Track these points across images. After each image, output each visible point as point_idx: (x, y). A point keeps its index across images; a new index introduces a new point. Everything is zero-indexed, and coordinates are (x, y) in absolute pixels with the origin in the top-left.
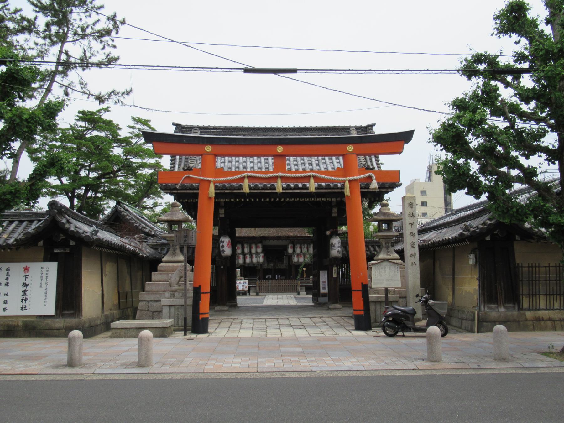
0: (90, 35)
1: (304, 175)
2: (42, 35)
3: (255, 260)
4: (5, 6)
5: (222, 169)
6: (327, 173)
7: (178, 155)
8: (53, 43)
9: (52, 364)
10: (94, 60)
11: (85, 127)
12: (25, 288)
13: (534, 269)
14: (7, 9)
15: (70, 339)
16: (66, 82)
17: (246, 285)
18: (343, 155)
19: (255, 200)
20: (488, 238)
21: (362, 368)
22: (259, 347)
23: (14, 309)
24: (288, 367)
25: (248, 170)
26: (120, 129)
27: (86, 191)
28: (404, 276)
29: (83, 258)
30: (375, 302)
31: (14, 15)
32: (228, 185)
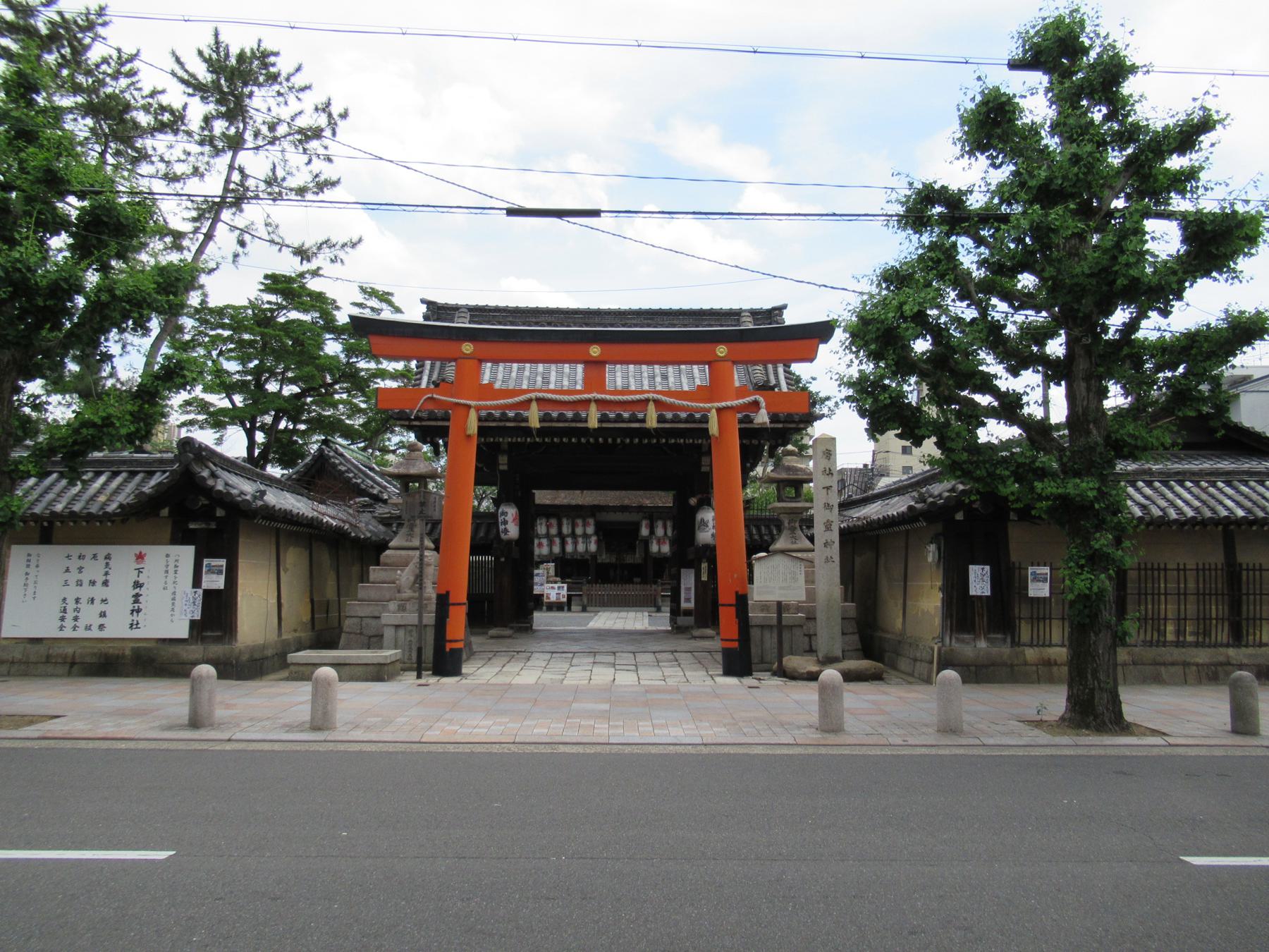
0: (284, 137)
1: (638, 397)
2: (197, 137)
3: (581, 548)
4: (133, 83)
5: (491, 384)
6: (680, 394)
7: (428, 359)
8: (217, 152)
9: (164, 722)
10: (292, 182)
11: (276, 304)
12: (137, 590)
13: (1213, 573)
14: (136, 89)
15: (194, 680)
16: (240, 221)
17: (564, 592)
18: (709, 363)
20: (959, 516)
21: (698, 741)
22: (537, 697)
23: (117, 627)
24: (572, 735)
25: (552, 386)
26: (338, 308)
27: (277, 420)
28: (810, 579)
29: (241, 540)
30: (762, 627)
31: (150, 100)
32: (511, 414)
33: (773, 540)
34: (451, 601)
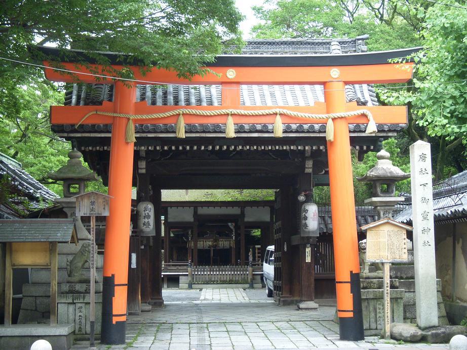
6: (307, 109)
18: (324, 84)
34: (116, 283)
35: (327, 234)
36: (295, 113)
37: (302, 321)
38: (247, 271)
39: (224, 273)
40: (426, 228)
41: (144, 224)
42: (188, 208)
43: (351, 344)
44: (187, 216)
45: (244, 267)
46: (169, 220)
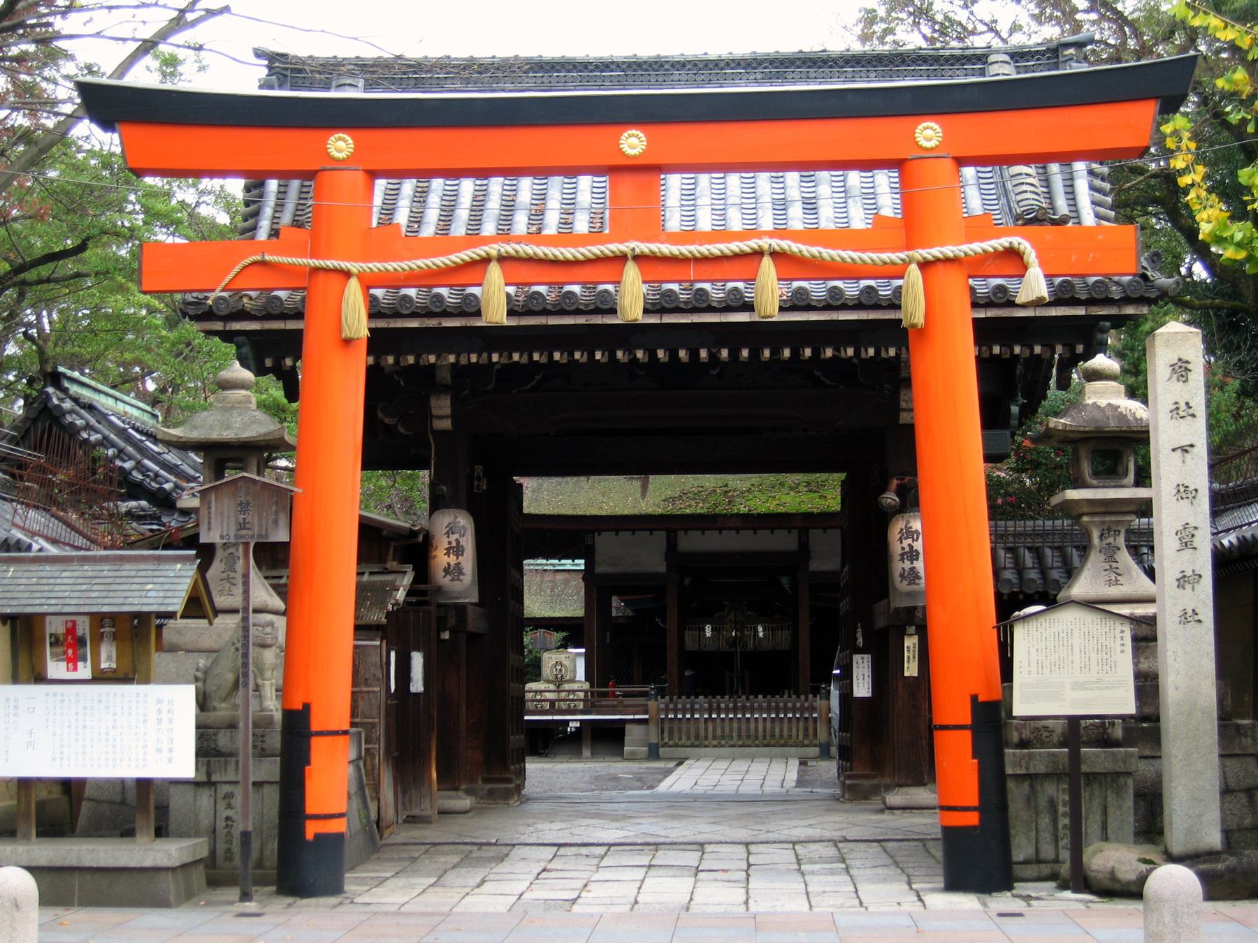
6: (844, 237)
18: (896, 164)
19: (734, 354)
33: (1071, 573)
34: (315, 726)
35: (1021, 597)
36: (815, 250)
37: (875, 841)
38: (813, 709)
39: (748, 716)
40: (1189, 573)
41: (447, 571)
42: (734, 532)
43: (967, 902)
44: (649, 557)
45: (807, 699)
46: (599, 569)
